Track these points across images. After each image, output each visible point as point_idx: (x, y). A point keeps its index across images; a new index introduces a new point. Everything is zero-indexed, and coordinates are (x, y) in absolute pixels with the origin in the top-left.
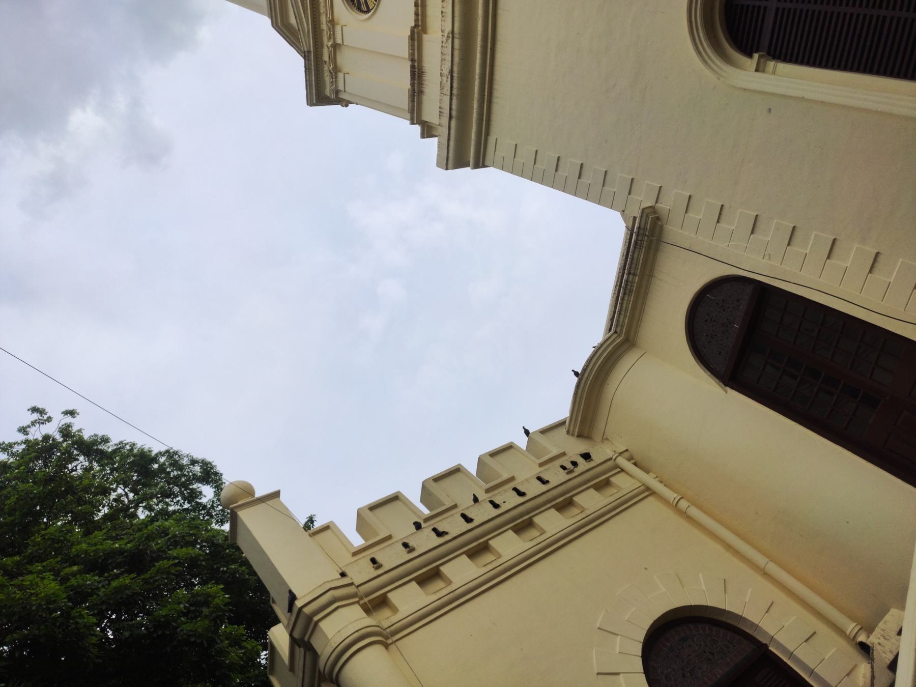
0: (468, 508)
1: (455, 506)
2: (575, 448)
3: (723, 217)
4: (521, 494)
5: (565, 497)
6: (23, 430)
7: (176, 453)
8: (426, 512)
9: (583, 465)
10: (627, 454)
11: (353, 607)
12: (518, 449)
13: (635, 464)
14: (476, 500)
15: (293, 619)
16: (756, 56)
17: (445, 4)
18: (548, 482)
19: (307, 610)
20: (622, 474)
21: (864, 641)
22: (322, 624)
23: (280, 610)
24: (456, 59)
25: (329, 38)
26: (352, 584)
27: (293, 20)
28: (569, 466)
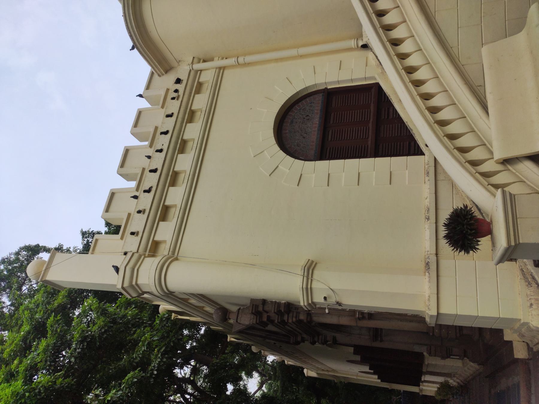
0: (149, 165)
2: (169, 81)
4: (166, 133)
5: (187, 113)
9: (181, 87)
10: (195, 60)
12: (147, 109)
13: (204, 61)
14: (149, 157)
18: (173, 113)
19: (126, 284)
20: (203, 72)
21: (362, 44)
22: (139, 282)
26: (133, 254)
28: (175, 95)
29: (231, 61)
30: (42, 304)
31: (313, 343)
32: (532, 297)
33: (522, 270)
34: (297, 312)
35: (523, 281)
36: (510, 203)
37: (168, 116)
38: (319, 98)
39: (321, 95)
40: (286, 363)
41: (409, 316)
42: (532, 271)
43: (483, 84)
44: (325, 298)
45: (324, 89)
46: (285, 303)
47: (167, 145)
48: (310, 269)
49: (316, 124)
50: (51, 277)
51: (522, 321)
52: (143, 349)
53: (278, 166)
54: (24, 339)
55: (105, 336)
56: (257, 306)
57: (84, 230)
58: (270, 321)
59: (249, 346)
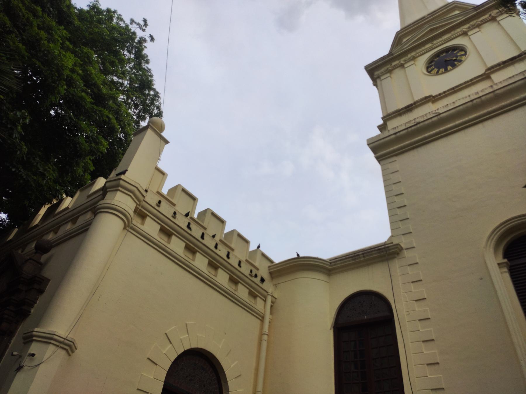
0: (208, 234)
2: (264, 272)
3: (416, 283)
6: (132, 21)
7: (159, 97)
8: (195, 216)
9: (258, 280)
10: (274, 299)
13: (271, 306)
14: (214, 236)
15: (114, 179)
16: (506, 260)
17: (452, 104)
18: (240, 267)
19: (122, 182)
20: (263, 302)
22: (119, 194)
23: (113, 175)
24: (427, 122)
25: (405, 61)
26: (144, 197)
27: (405, 40)
28: (254, 274)
29: (266, 329)
37: (240, 262)
44: (33, 355)
46: (30, 312)
48: (68, 347)
52: (41, 169)
54: (95, 85)
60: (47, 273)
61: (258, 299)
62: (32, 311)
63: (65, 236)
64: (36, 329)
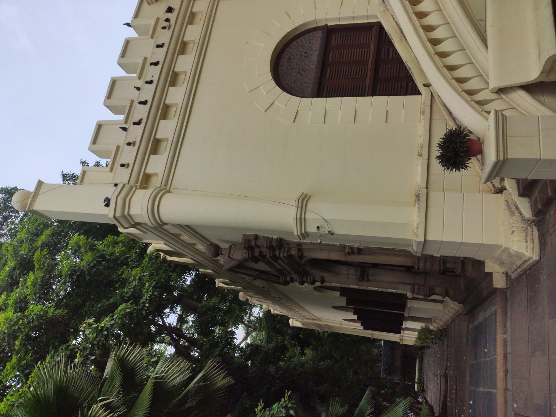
0: (139, 97)
1: (132, 102)
4: (156, 64)
8: (121, 117)
9: (172, 16)
11: (136, 193)
12: (134, 39)
14: (138, 89)
18: (163, 44)
19: (118, 214)
22: (131, 213)
26: (124, 185)
28: (166, 24)
30: (26, 241)
31: (302, 283)
32: (514, 225)
33: (507, 201)
34: (288, 248)
35: (507, 211)
36: (502, 122)
37: (158, 46)
38: (319, 35)
39: (320, 31)
40: (272, 312)
41: (396, 250)
42: (516, 200)
43: (484, 19)
44: (318, 228)
45: (324, 26)
46: (277, 238)
47: (158, 76)
48: (304, 201)
49: (314, 61)
50: (39, 206)
51: (503, 247)
52: (134, 283)
53: (273, 102)
54: (10, 276)
55: (95, 270)
56: (249, 241)
57: (64, 173)
58: (262, 256)
59: (236, 293)
60: (238, 238)
61: (194, 10)
62: (276, 237)
63: (197, 237)
64: (295, 233)
